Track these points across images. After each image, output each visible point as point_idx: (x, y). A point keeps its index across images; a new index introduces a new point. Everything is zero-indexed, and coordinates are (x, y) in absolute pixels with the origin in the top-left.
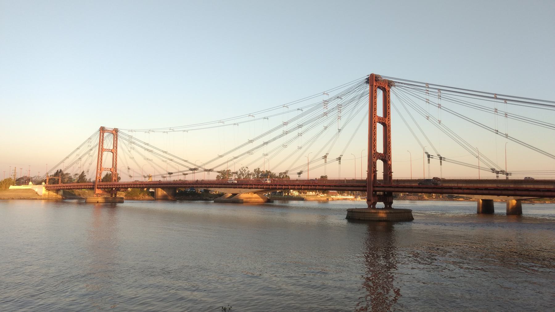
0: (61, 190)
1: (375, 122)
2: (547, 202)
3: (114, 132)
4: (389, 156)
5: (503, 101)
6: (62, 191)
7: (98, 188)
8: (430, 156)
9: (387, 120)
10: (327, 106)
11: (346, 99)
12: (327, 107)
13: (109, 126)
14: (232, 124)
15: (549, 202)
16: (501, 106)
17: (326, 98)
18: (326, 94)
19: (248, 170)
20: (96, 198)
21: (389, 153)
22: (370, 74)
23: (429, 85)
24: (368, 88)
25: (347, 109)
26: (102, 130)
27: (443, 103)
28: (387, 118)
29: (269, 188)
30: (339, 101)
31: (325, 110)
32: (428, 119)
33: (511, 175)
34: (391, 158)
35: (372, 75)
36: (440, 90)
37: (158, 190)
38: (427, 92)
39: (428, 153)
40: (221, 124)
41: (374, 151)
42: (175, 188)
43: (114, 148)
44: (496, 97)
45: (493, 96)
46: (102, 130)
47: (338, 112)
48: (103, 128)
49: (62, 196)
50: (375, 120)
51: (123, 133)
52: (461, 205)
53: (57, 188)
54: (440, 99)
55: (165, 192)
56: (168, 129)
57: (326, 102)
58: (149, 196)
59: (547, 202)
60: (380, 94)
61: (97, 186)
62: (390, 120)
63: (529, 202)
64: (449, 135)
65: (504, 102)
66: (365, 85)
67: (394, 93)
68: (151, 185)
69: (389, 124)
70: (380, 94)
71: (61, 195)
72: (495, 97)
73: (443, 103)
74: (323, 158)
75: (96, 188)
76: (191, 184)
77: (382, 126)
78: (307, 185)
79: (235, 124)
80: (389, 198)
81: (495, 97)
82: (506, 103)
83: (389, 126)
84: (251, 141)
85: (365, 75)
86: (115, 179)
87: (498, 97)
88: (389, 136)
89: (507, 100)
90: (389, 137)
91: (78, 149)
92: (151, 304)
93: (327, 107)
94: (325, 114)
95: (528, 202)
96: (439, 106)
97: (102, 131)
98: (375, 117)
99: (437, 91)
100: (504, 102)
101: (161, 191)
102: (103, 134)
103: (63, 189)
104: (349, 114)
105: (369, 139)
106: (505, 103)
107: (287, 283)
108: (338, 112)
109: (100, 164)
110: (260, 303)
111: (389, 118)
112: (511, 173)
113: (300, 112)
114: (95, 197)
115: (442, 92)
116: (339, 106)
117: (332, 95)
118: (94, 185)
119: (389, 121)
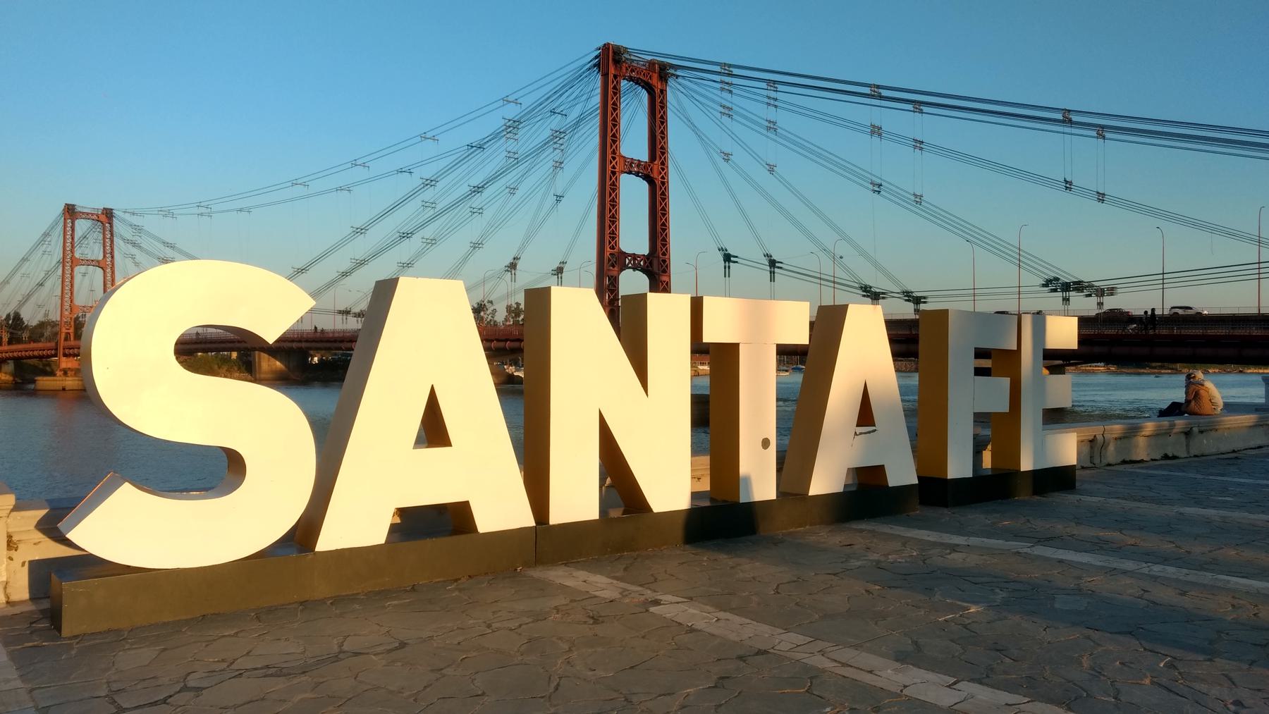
0: (9, 361)
1: (614, 173)
2: (1210, 371)
3: (103, 218)
4: (664, 261)
5: (910, 107)
6: (11, 363)
7: (65, 355)
8: (732, 259)
9: (655, 167)
12: (516, 137)
13: (90, 201)
14: (330, 191)
15: (1217, 371)
16: (897, 120)
17: (512, 112)
18: (513, 102)
19: (492, 308)
20: (61, 378)
21: (664, 254)
22: (601, 44)
23: (731, 69)
24: (597, 81)
26: (71, 212)
27: (784, 119)
28: (656, 162)
29: (504, 349)
32: (727, 160)
33: (925, 302)
34: (668, 267)
35: (606, 47)
36: (774, 81)
37: (260, 358)
38: (728, 88)
39: (771, 256)
40: (299, 190)
41: (613, 248)
42: (303, 354)
43: (104, 256)
44: (880, 93)
45: (1059, 116)
46: (71, 212)
48: (70, 207)
49: (14, 375)
50: (614, 167)
51: (123, 221)
53: (7, 355)
54: (776, 106)
55: (278, 363)
56: (192, 205)
57: (513, 126)
58: (240, 372)
59: (1210, 371)
61: (64, 349)
62: (668, 167)
63: (1170, 371)
64: (945, 219)
65: (1096, 135)
67: (674, 95)
68: (236, 343)
69: (663, 178)
71: (11, 374)
72: (876, 93)
73: (784, 119)
74: (553, 272)
75: (61, 353)
76: (234, 342)
77: (645, 186)
78: (503, 338)
79: (341, 189)
81: (876, 93)
82: (921, 112)
83: (663, 183)
84: (361, 231)
85: (589, 51)
86: (67, 331)
87: (885, 93)
88: (663, 209)
89: (1103, 127)
90: (665, 212)
91: (24, 260)
93: (516, 137)
95: (1167, 371)
96: (772, 127)
97: (68, 216)
98: (614, 158)
99: (764, 85)
100: (912, 109)
101: (269, 359)
102: (73, 223)
103: (14, 359)
105: (598, 217)
106: (914, 112)
109: (67, 297)
111: (663, 163)
112: (925, 298)
114: (60, 376)
115: (780, 87)
118: (56, 349)
119: (663, 169)
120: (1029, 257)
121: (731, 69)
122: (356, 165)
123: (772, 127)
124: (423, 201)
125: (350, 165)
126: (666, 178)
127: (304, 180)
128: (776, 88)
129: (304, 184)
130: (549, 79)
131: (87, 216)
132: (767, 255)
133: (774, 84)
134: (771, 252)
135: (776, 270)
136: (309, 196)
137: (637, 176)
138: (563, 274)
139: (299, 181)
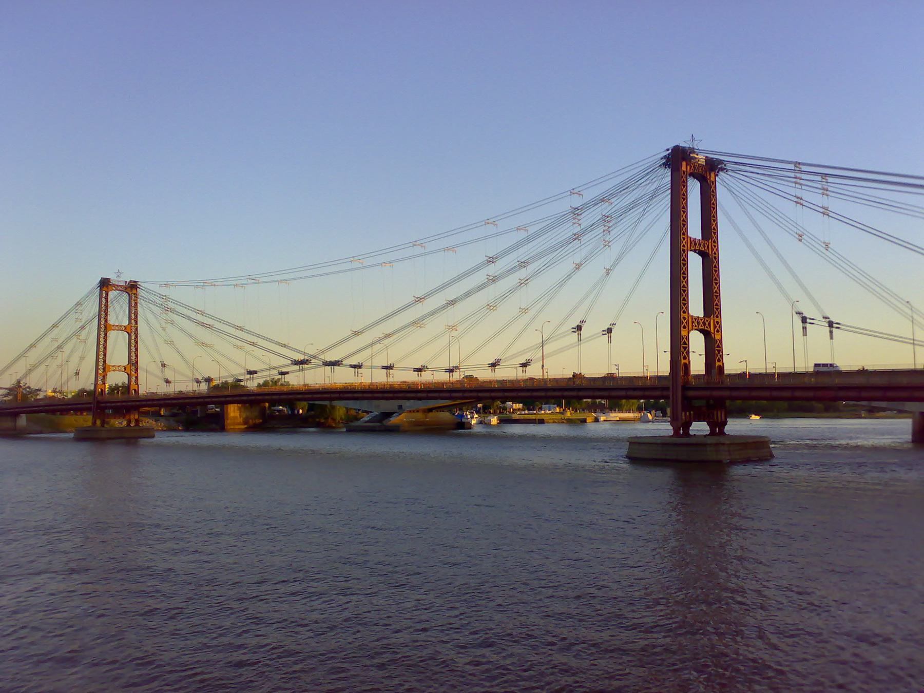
10: (579, 220)
11: (621, 202)
12: (580, 222)
14: (439, 250)
17: (577, 202)
22: (671, 145)
26: (105, 284)
27: (834, 204)
30: (604, 208)
31: (577, 229)
38: (797, 181)
40: (418, 250)
46: (105, 284)
54: (827, 195)
57: (576, 212)
60: (694, 189)
70: (694, 189)
85: (662, 148)
91: (55, 326)
99: (819, 178)
115: (830, 179)
120: (854, 330)
121: (801, 166)
122: (488, 223)
123: (825, 212)
124: (487, 275)
125: (484, 223)
126: (717, 254)
127: (422, 242)
128: (827, 180)
129: (494, 223)
130: (631, 168)
131: (117, 287)
132: (799, 313)
133: (826, 176)
134: (801, 310)
135: (448, 368)
136: (425, 254)
137: (695, 252)
138: (612, 334)
139: (417, 243)
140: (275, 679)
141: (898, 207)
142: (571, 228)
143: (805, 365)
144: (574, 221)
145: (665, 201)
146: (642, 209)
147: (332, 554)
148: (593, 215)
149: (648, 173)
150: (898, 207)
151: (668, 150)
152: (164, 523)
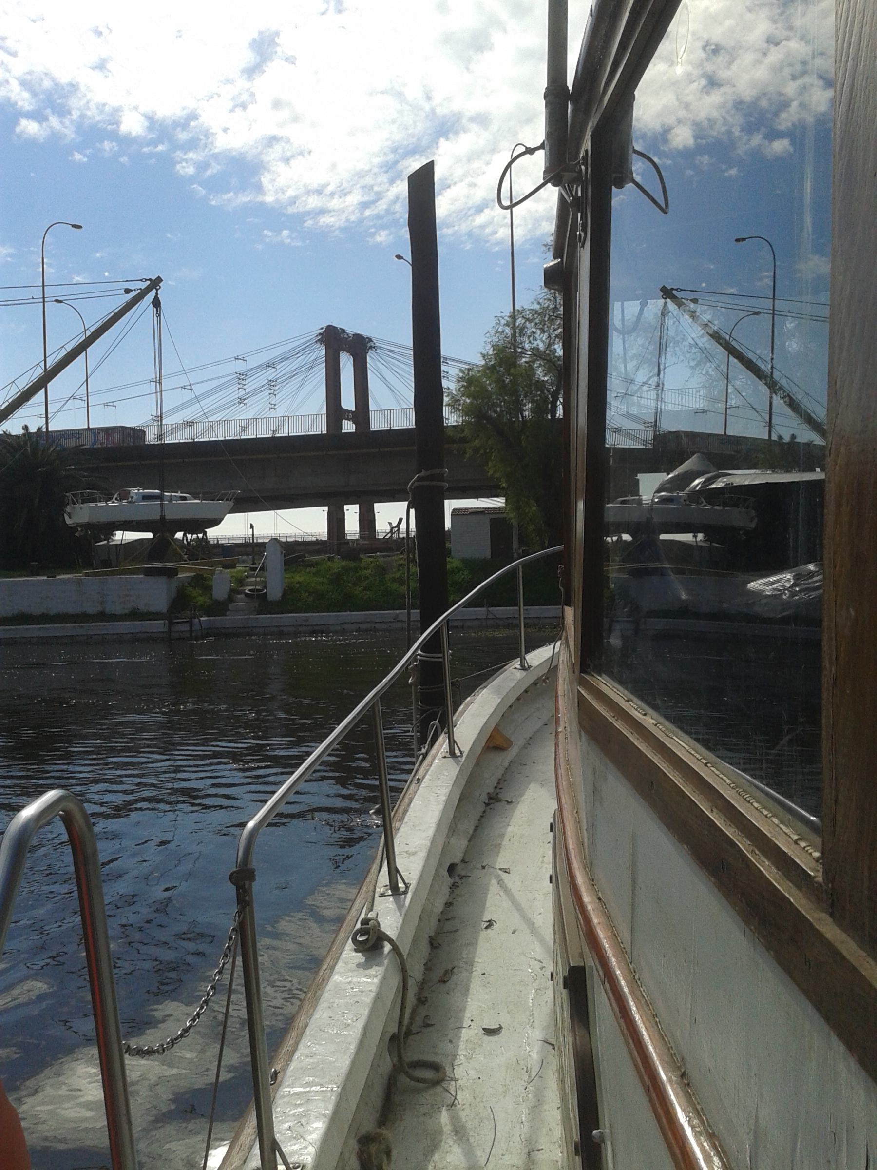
10: (244, 385)
11: (283, 369)
12: (245, 387)
17: (240, 367)
22: (324, 325)
25: (287, 390)
30: (271, 374)
31: (242, 393)
47: (270, 394)
52: (252, 961)
57: (241, 377)
60: (346, 364)
66: (318, 345)
70: (346, 364)
80: (644, 502)
92: (248, 774)
93: (245, 387)
94: (241, 400)
104: (288, 402)
107: (402, 1040)
108: (270, 394)
110: (657, 1095)
113: (188, 395)
116: (271, 384)
117: (253, 362)
140: (688, 95)
141: (259, 792)
142: (237, 392)
143: (373, 1056)
144: (239, 386)
145: (320, 374)
146: (303, 377)
147: (119, 851)
148: (261, 379)
149: (304, 349)
150: (259, 792)
151: (322, 328)
152: (335, 203)
